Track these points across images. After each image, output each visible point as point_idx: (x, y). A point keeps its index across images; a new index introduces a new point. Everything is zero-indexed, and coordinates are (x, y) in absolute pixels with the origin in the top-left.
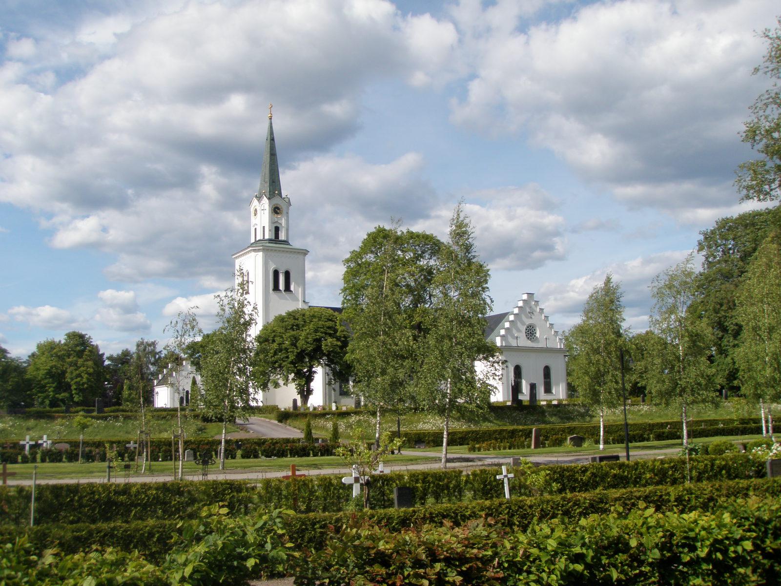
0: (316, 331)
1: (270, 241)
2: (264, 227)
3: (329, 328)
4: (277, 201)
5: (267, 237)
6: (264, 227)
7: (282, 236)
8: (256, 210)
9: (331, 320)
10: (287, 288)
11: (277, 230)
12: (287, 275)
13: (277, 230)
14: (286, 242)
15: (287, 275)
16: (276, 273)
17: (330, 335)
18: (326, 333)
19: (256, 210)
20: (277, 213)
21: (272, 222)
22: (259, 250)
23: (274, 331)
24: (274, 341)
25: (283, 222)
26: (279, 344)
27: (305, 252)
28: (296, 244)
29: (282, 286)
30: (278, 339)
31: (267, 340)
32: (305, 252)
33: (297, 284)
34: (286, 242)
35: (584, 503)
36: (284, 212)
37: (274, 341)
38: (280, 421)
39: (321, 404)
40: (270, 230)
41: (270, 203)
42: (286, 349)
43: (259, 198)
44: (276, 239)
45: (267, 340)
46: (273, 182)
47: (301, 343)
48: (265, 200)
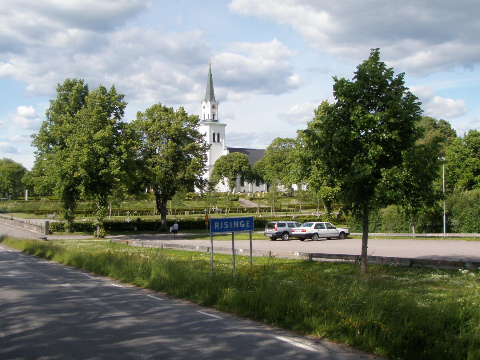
0: (239, 163)
1: (211, 120)
2: (208, 115)
3: (244, 162)
4: (214, 103)
5: (210, 118)
6: (208, 115)
7: (216, 118)
8: (204, 106)
9: (244, 159)
10: (218, 141)
11: (214, 115)
12: (218, 135)
13: (214, 115)
14: (217, 121)
15: (218, 135)
16: (214, 134)
17: (244, 164)
18: (243, 164)
19: (204, 106)
20: (213, 108)
21: (212, 112)
22: (207, 125)
23: (223, 163)
24: (223, 167)
25: (216, 112)
26: (225, 168)
27: (225, 125)
28: (221, 122)
29: (216, 140)
30: (225, 166)
31: (220, 166)
32: (225, 125)
33: (222, 139)
34: (217, 121)
35: (327, 117)
36: (217, 107)
37: (223, 167)
38: (251, 200)
39: (208, 126)
40: (211, 116)
41: (211, 104)
42: (228, 170)
43: (206, 101)
44: (213, 120)
45: (220, 166)
46: (212, 94)
47: (234, 168)
48: (209, 103)
